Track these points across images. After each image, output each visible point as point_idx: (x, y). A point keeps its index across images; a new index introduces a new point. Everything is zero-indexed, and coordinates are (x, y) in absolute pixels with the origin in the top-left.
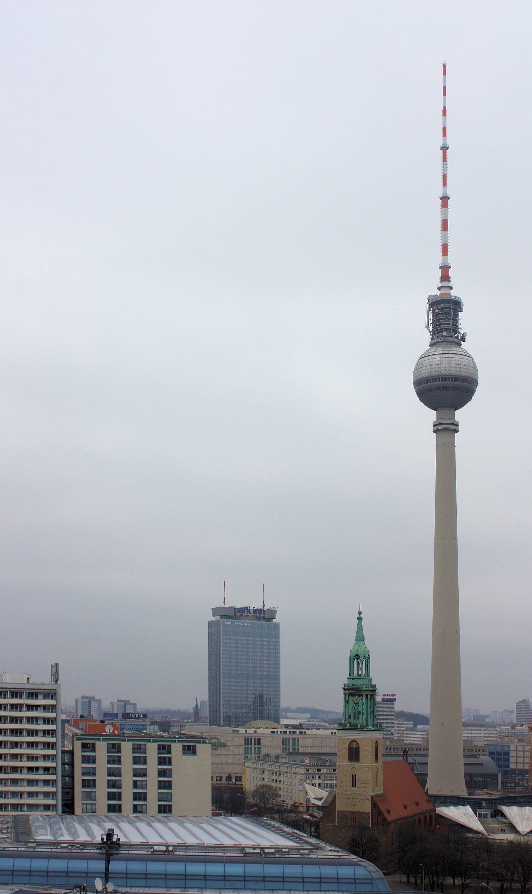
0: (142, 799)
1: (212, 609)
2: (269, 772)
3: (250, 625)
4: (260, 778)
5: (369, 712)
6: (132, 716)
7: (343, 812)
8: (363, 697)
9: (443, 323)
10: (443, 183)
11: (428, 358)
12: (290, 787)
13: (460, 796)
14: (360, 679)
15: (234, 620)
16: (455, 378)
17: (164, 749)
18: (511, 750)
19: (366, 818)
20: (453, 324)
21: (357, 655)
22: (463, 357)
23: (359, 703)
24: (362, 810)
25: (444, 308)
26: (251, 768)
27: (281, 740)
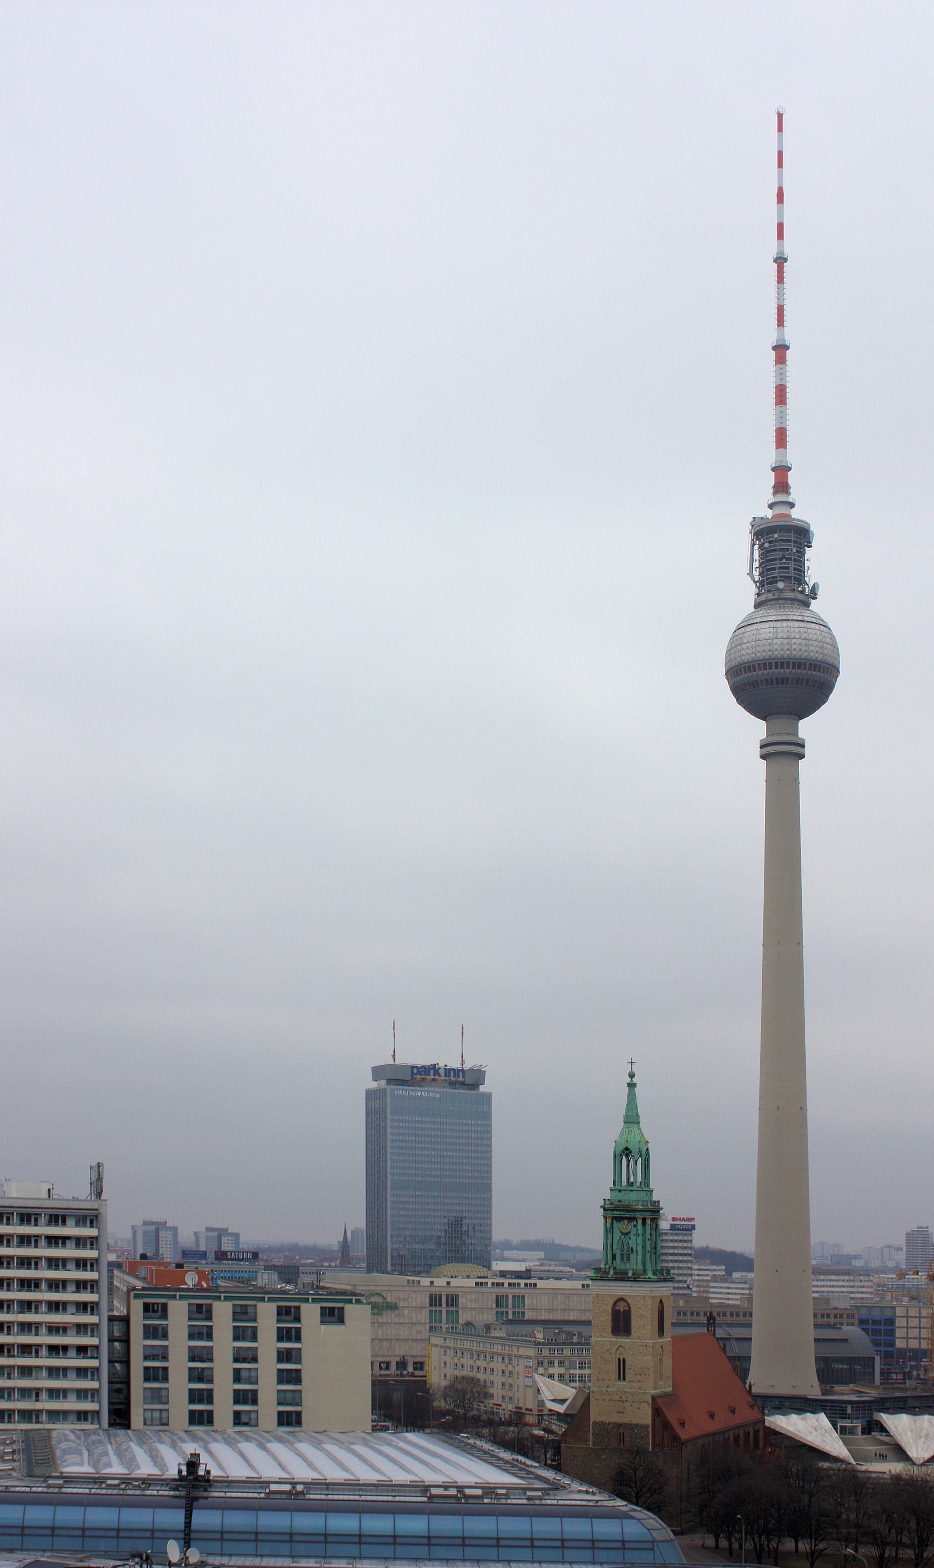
0: (250, 1401)
1: (372, 1068)
2: (472, 1355)
3: (438, 1095)
4: (456, 1365)
5: (648, 1248)
6: (231, 1255)
7: (603, 1424)
8: (637, 1222)
9: (778, 566)
10: (778, 321)
11: (752, 627)
12: (510, 1380)
13: (808, 1397)
14: (632, 1191)
15: (411, 1088)
16: (798, 662)
17: (288, 1313)
18: (897, 1315)
19: (642, 1434)
20: (795, 569)
21: (627, 1149)
22: (813, 626)
23: (630, 1232)
24: (635, 1421)
25: (780, 540)
26: (441, 1347)
27: (494, 1297)
